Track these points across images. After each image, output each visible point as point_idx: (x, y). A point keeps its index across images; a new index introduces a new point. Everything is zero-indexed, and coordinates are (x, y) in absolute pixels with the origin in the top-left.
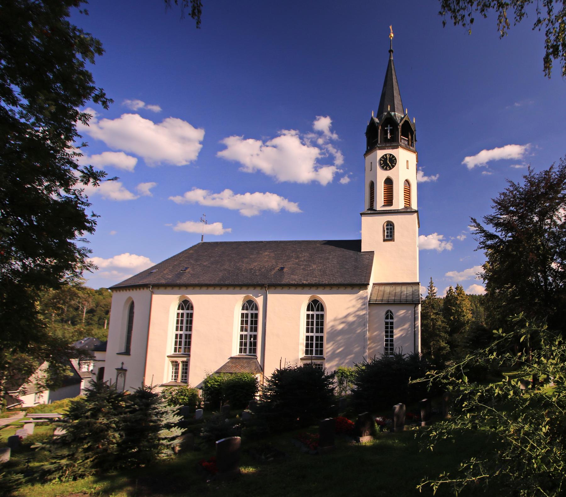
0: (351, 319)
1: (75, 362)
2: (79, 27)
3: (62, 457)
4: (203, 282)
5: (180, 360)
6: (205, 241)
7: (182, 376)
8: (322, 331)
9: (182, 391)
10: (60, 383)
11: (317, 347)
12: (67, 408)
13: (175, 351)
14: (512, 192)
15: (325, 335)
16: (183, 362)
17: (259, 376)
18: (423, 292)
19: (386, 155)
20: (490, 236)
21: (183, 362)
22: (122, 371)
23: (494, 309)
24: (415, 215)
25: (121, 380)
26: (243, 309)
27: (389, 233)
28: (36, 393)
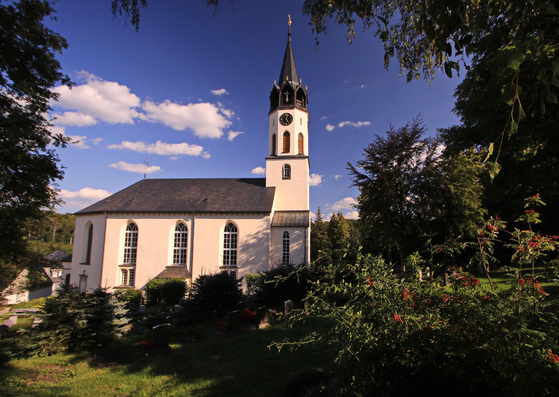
0: (260, 236)
1: (47, 270)
2: (50, 29)
3: (40, 339)
4: (145, 210)
5: (128, 269)
6: (147, 178)
7: (130, 281)
8: (236, 247)
9: (129, 292)
10: (37, 286)
11: (232, 258)
12: (44, 304)
13: (125, 261)
14: (378, 143)
15: (239, 249)
16: (130, 270)
17: (188, 281)
18: (312, 217)
19: (285, 114)
20: (361, 177)
21: (130, 270)
22: (84, 277)
23: (365, 230)
24: (307, 159)
25: (83, 283)
26: (176, 230)
27: (287, 173)
28: (18, 294)
